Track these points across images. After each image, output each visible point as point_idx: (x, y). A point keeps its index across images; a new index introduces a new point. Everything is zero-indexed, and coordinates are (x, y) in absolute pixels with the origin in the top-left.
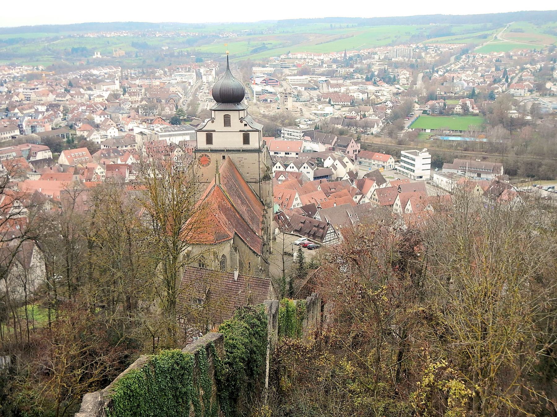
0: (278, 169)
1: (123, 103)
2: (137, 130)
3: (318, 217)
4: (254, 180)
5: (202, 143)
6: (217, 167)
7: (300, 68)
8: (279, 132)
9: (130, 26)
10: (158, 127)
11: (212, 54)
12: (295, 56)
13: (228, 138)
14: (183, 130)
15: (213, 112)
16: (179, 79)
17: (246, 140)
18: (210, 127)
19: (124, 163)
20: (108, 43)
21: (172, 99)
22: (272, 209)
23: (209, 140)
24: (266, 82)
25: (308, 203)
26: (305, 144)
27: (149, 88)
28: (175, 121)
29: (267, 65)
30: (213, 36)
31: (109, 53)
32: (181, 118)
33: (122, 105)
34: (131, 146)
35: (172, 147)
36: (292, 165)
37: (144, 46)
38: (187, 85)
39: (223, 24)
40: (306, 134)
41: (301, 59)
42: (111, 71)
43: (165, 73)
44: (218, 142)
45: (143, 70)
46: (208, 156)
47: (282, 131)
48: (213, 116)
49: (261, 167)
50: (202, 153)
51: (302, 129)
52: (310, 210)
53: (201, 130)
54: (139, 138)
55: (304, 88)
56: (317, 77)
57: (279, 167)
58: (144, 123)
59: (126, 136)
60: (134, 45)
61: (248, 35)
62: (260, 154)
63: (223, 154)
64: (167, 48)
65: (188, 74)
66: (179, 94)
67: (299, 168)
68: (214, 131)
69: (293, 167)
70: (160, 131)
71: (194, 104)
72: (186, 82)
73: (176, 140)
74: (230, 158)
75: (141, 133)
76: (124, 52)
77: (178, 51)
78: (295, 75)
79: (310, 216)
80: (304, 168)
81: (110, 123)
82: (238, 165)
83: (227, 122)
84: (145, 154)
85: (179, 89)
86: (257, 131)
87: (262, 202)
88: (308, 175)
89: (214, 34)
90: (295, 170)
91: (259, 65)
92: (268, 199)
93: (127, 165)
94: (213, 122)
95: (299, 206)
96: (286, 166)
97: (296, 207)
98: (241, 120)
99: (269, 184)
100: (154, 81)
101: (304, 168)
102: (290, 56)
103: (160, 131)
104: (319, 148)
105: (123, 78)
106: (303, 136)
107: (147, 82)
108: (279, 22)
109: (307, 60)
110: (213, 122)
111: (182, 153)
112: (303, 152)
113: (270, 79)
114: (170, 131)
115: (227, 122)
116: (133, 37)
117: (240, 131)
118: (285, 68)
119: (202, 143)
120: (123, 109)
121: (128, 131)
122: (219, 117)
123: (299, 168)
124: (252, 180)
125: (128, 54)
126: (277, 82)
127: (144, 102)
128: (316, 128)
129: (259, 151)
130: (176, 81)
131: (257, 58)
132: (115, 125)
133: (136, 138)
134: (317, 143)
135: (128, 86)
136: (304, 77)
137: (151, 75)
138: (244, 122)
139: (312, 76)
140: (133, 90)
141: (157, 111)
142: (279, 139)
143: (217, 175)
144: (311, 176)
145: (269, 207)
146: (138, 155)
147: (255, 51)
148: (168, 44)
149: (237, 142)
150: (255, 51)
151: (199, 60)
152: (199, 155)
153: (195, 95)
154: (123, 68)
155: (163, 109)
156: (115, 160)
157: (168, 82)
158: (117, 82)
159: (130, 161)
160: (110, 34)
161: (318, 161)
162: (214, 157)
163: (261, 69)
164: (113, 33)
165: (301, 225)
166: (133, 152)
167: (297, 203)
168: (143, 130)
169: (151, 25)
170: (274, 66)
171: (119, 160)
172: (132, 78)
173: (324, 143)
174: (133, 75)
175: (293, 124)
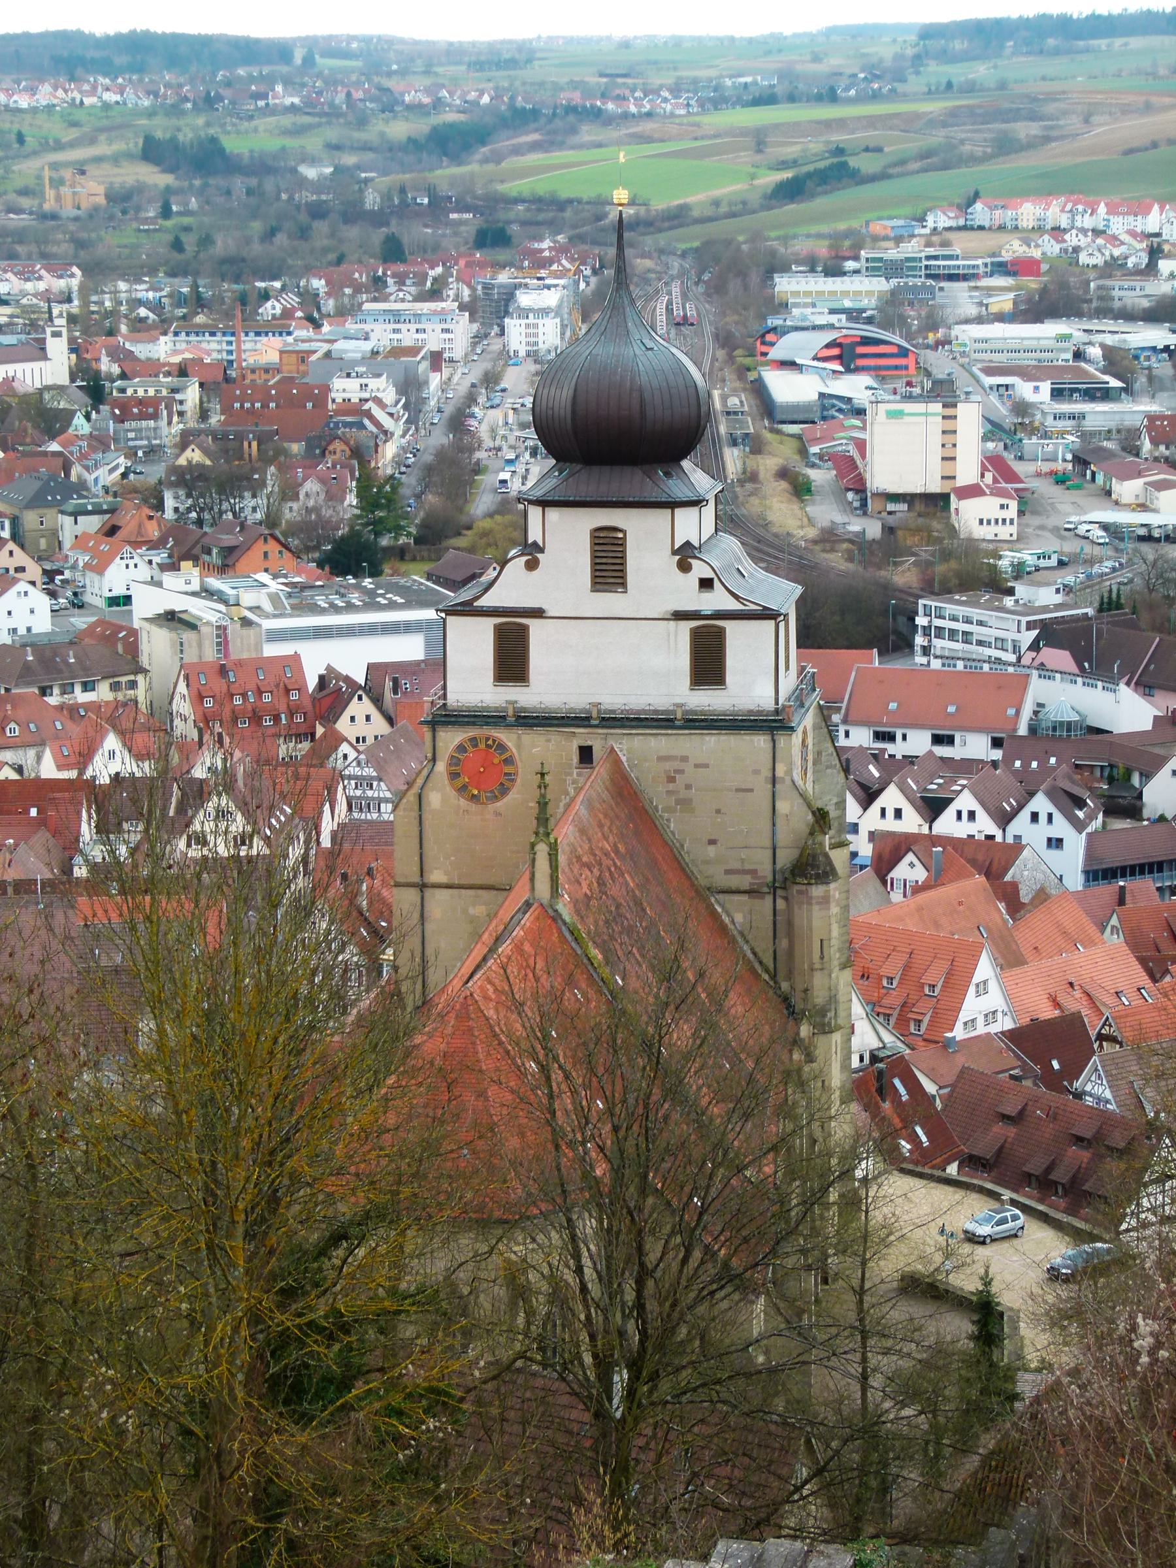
0: (890, 825)
1: (83, 457)
2: (148, 604)
3: (1096, 1087)
4: (745, 882)
5: (471, 679)
6: (543, 805)
7: (1032, 283)
8: (902, 620)
9: (137, 53)
10: (259, 588)
11: (561, 205)
12: (999, 216)
13: (606, 647)
14: (392, 606)
15: (534, 513)
16: (382, 336)
17: (708, 663)
18: (511, 587)
19: (72, 774)
20: (21, 139)
21: (334, 434)
22: (837, 1037)
23: (511, 661)
24: (846, 355)
25: (1048, 1013)
26: (1038, 689)
27: (221, 382)
28: (350, 558)
29: (850, 265)
30: (571, 109)
31: (25, 192)
32: (385, 541)
33: (76, 471)
34: (115, 687)
35: (333, 694)
36: (966, 801)
37: (207, 160)
38: (424, 366)
39: (625, 45)
40: (1051, 633)
41: (1039, 230)
42: (29, 286)
43: (310, 299)
44: (560, 674)
45: (195, 286)
46: (502, 747)
47: (921, 621)
48: (534, 535)
49: (783, 807)
50: (472, 732)
51: (1029, 609)
52: (1055, 1045)
53: (467, 610)
54: (157, 646)
55: (1046, 387)
56: (1120, 325)
57: (898, 813)
58: (186, 565)
59: (92, 627)
60: (152, 152)
61: (758, 102)
62: (782, 741)
63: (583, 736)
64: (329, 170)
65: (426, 307)
66: (377, 412)
67: (1004, 819)
68: (538, 613)
69: (972, 815)
70: (267, 606)
71: (454, 468)
72: (413, 351)
73: (352, 659)
74: (617, 762)
75: (171, 618)
76: (101, 190)
77: (384, 182)
78: (1001, 318)
79: (1054, 1081)
80: (1035, 817)
81: (12, 564)
82: (657, 795)
83: (609, 565)
84: (184, 729)
85: (384, 388)
86: (766, 614)
87: (786, 1000)
88: (1052, 856)
89: (576, 98)
90: (985, 825)
91: (812, 265)
92: (818, 980)
93: (90, 787)
94: (532, 565)
95: (995, 1028)
96: (933, 807)
97: (981, 1029)
98: (685, 555)
99: (825, 901)
100: (248, 343)
101: (1035, 817)
102: (980, 212)
103: (267, 606)
104: (1128, 711)
105: (90, 328)
106: (1035, 647)
107: (213, 349)
108: (929, 33)
109: (1072, 239)
110: (532, 565)
111: (380, 726)
112: (1033, 730)
113: (866, 341)
114: (322, 611)
115: (609, 565)
116: (151, 113)
117: (679, 616)
118: (952, 278)
119: (471, 679)
120: (81, 487)
121: (100, 603)
122: (567, 536)
123: (1004, 819)
124: (735, 881)
125: (122, 200)
126: (903, 353)
127: (194, 455)
128: (1109, 605)
129: (773, 724)
130: (367, 346)
131: (808, 227)
132: (34, 570)
133: (144, 647)
134: (1111, 680)
135: (116, 369)
136: (1050, 329)
137: (243, 313)
138: (700, 570)
139: (1094, 325)
140: (138, 389)
141: (262, 501)
142: (898, 665)
143: (542, 849)
144: (1070, 864)
145: (825, 1029)
146: (147, 728)
147: (791, 191)
148: (335, 147)
149: (655, 672)
150: (791, 191)
151: (493, 238)
152: (451, 739)
153: (458, 422)
154: (98, 271)
155: (289, 492)
156: (27, 757)
157: (325, 347)
158: (58, 348)
159: (111, 761)
160: (32, 91)
161: (1111, 780)
162: (531, 749)
163: (820, 284)
164: (46, 88)
165: (1000, 1130)
166: (118, 717)
167: (987, 1007)
168: (179, 603)
169: (247, 50)
170: (891, 269)
171: (48, 756)
172: (138, 326)
173: (1146, 687)
174: (143, 312)
175: (982, 579)
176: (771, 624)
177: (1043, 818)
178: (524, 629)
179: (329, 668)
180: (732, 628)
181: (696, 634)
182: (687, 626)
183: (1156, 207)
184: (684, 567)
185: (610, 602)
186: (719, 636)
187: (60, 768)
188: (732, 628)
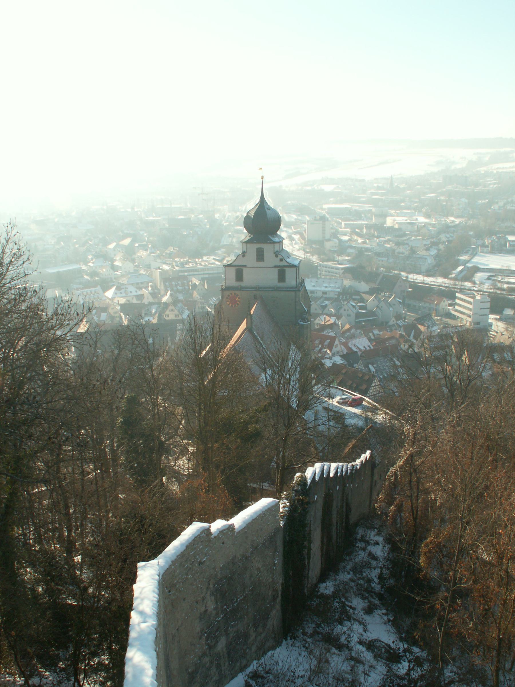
80: (345, 310)
101: (345, 310)
176: (295, 268)
177: (346, 310)
178: (242, 270)
179: (264, 261)
180: (287, 269)
181: (279, 271)
182: (277, 269)
183: (284, 640)
184: (277, 256)
185: (260, 264)
186: (284, 271)
187: (137, 300)
188: (287, 269)
